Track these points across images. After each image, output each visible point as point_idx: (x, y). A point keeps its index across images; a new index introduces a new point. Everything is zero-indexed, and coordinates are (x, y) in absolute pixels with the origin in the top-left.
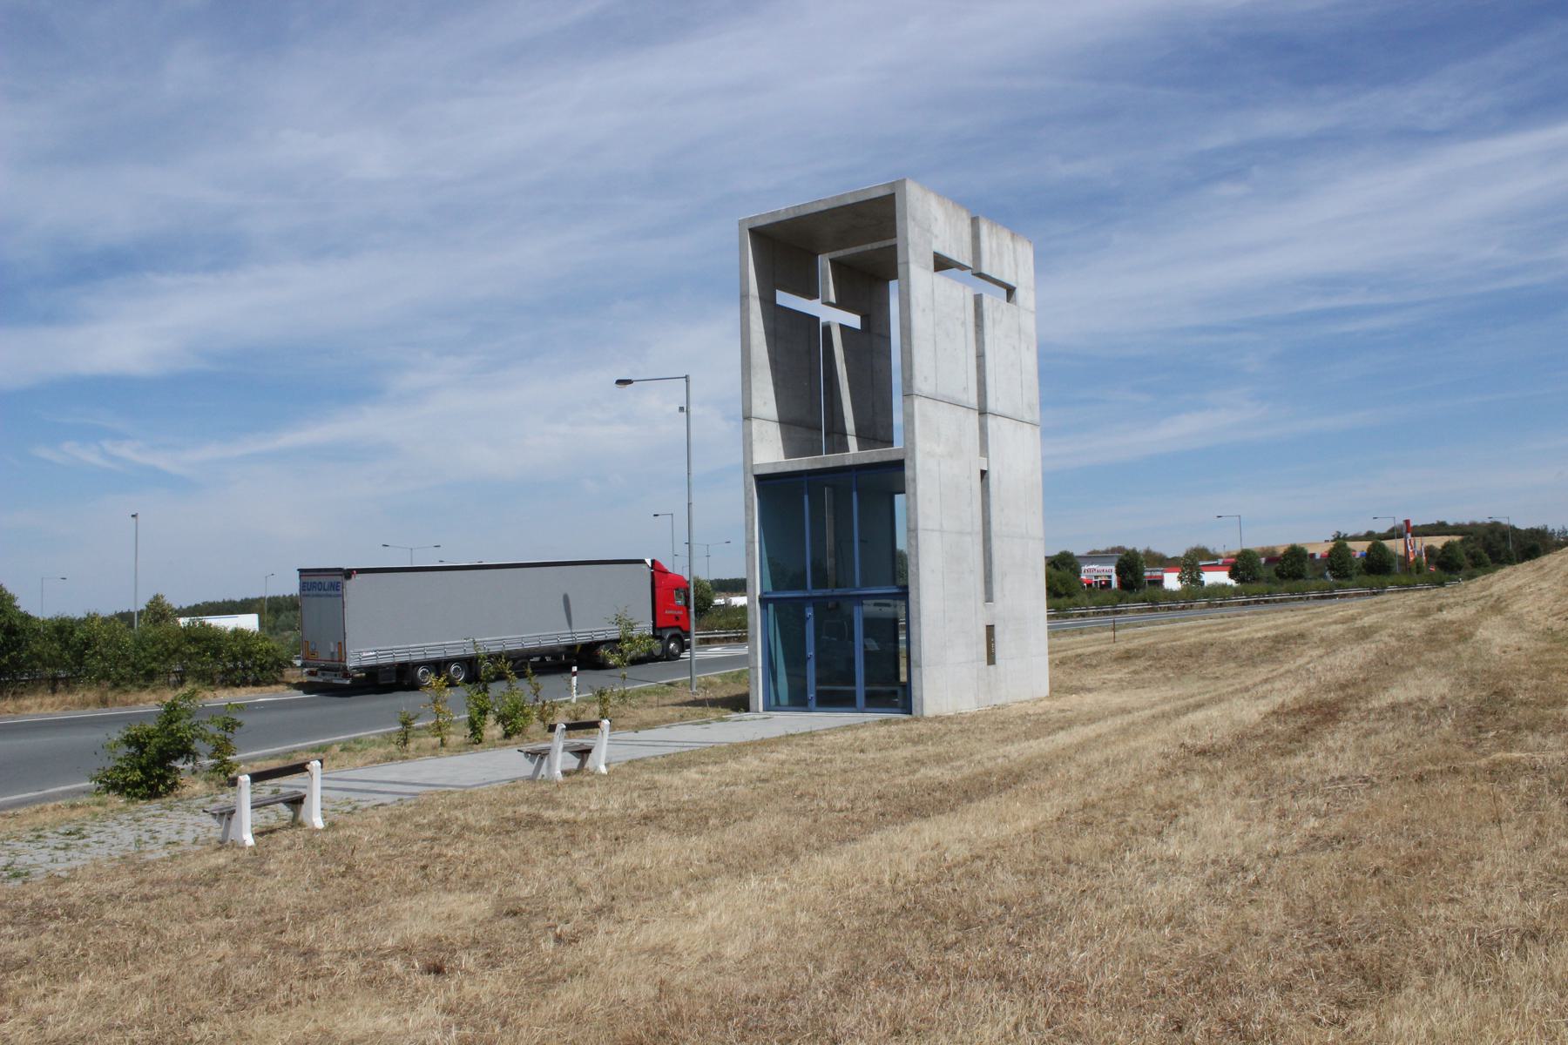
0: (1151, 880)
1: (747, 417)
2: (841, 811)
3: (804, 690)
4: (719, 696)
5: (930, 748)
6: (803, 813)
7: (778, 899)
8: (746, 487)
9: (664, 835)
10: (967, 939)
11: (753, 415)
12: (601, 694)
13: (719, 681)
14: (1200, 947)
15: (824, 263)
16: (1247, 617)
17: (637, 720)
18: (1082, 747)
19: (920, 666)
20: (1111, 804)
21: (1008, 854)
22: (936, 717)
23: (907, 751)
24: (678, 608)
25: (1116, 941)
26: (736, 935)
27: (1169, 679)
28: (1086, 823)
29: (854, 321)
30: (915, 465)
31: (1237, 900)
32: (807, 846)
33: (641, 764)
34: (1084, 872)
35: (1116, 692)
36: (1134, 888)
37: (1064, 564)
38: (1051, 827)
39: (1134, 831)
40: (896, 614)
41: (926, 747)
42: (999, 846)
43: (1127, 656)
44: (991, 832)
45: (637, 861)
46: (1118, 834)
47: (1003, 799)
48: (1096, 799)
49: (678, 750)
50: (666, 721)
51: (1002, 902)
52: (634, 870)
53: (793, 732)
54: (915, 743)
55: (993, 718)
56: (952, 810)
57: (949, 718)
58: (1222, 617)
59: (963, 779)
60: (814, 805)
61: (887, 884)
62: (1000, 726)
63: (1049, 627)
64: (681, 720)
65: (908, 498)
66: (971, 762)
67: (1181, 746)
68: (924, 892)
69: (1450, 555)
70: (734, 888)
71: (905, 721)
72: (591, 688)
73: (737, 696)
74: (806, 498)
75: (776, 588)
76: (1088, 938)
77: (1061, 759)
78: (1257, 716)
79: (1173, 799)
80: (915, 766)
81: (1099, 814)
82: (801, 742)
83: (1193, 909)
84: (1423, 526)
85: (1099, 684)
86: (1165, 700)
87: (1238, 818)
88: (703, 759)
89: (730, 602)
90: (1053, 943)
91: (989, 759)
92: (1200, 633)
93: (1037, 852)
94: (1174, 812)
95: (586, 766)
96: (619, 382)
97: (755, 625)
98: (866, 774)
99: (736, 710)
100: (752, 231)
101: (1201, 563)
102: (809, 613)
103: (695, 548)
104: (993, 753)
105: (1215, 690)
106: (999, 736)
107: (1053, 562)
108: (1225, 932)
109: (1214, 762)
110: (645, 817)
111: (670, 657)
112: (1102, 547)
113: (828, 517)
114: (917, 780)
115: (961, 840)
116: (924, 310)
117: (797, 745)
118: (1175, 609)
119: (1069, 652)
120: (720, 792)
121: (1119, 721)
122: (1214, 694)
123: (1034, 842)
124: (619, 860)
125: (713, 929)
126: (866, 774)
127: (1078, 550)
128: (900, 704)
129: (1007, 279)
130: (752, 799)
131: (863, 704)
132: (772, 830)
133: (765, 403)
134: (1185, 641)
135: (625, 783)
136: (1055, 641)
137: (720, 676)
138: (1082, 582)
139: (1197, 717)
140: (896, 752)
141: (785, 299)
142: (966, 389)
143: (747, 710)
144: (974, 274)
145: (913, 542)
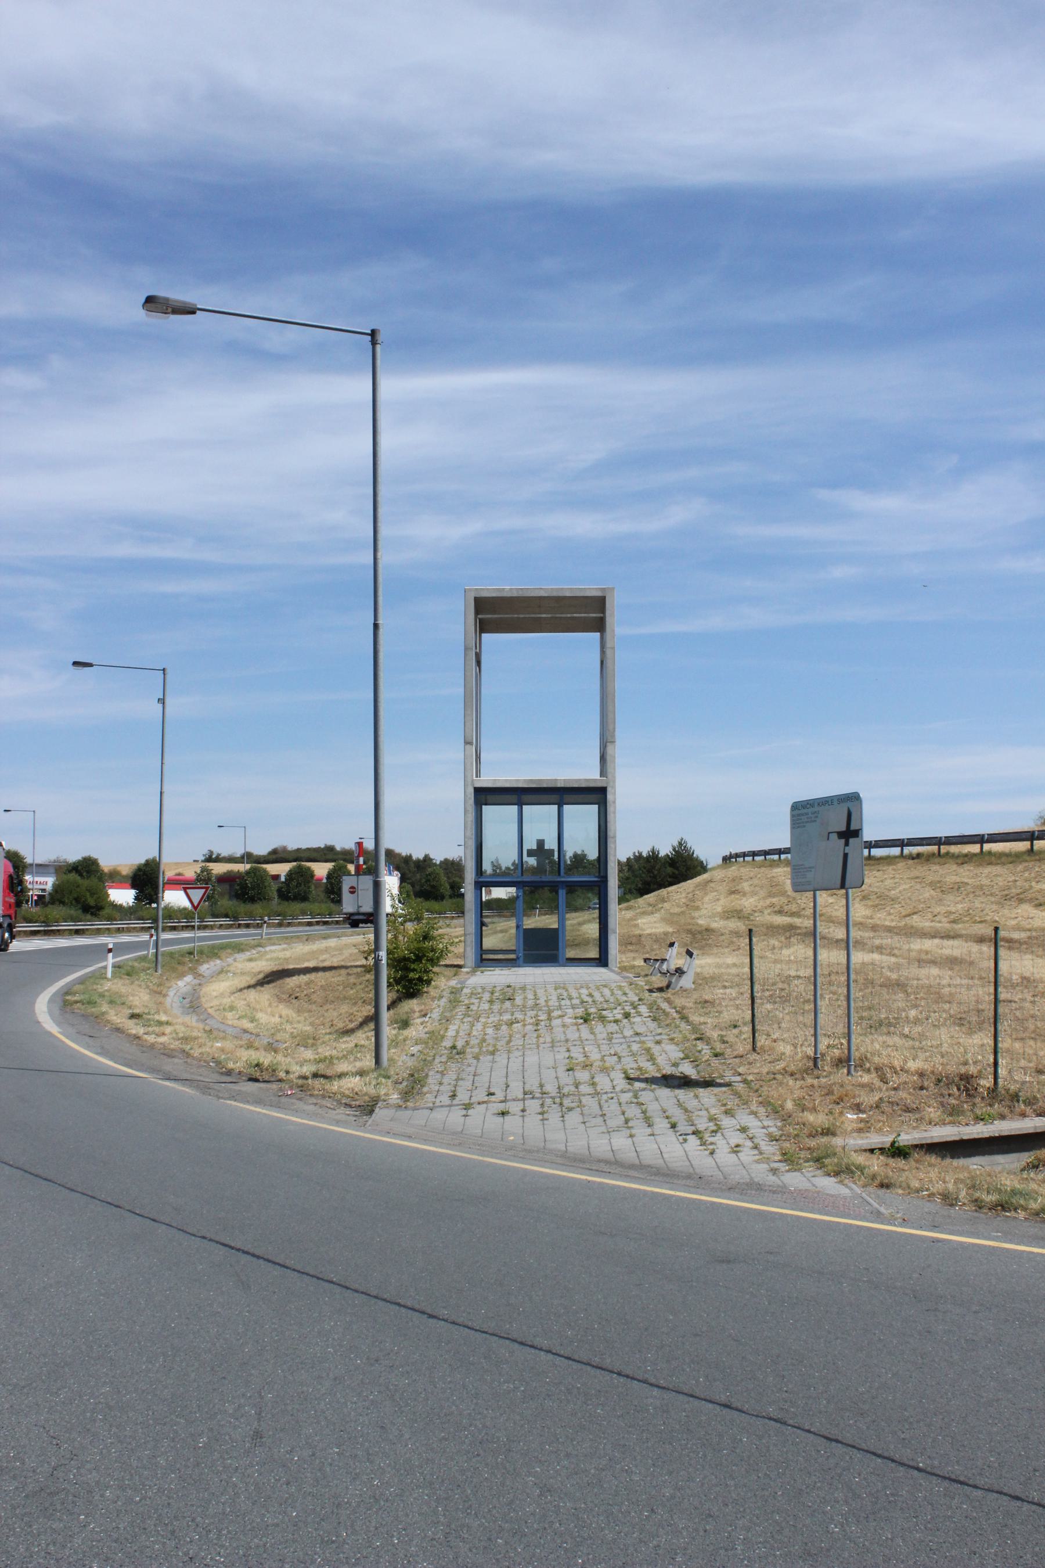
69: (434, 883)
84: (308, 849)
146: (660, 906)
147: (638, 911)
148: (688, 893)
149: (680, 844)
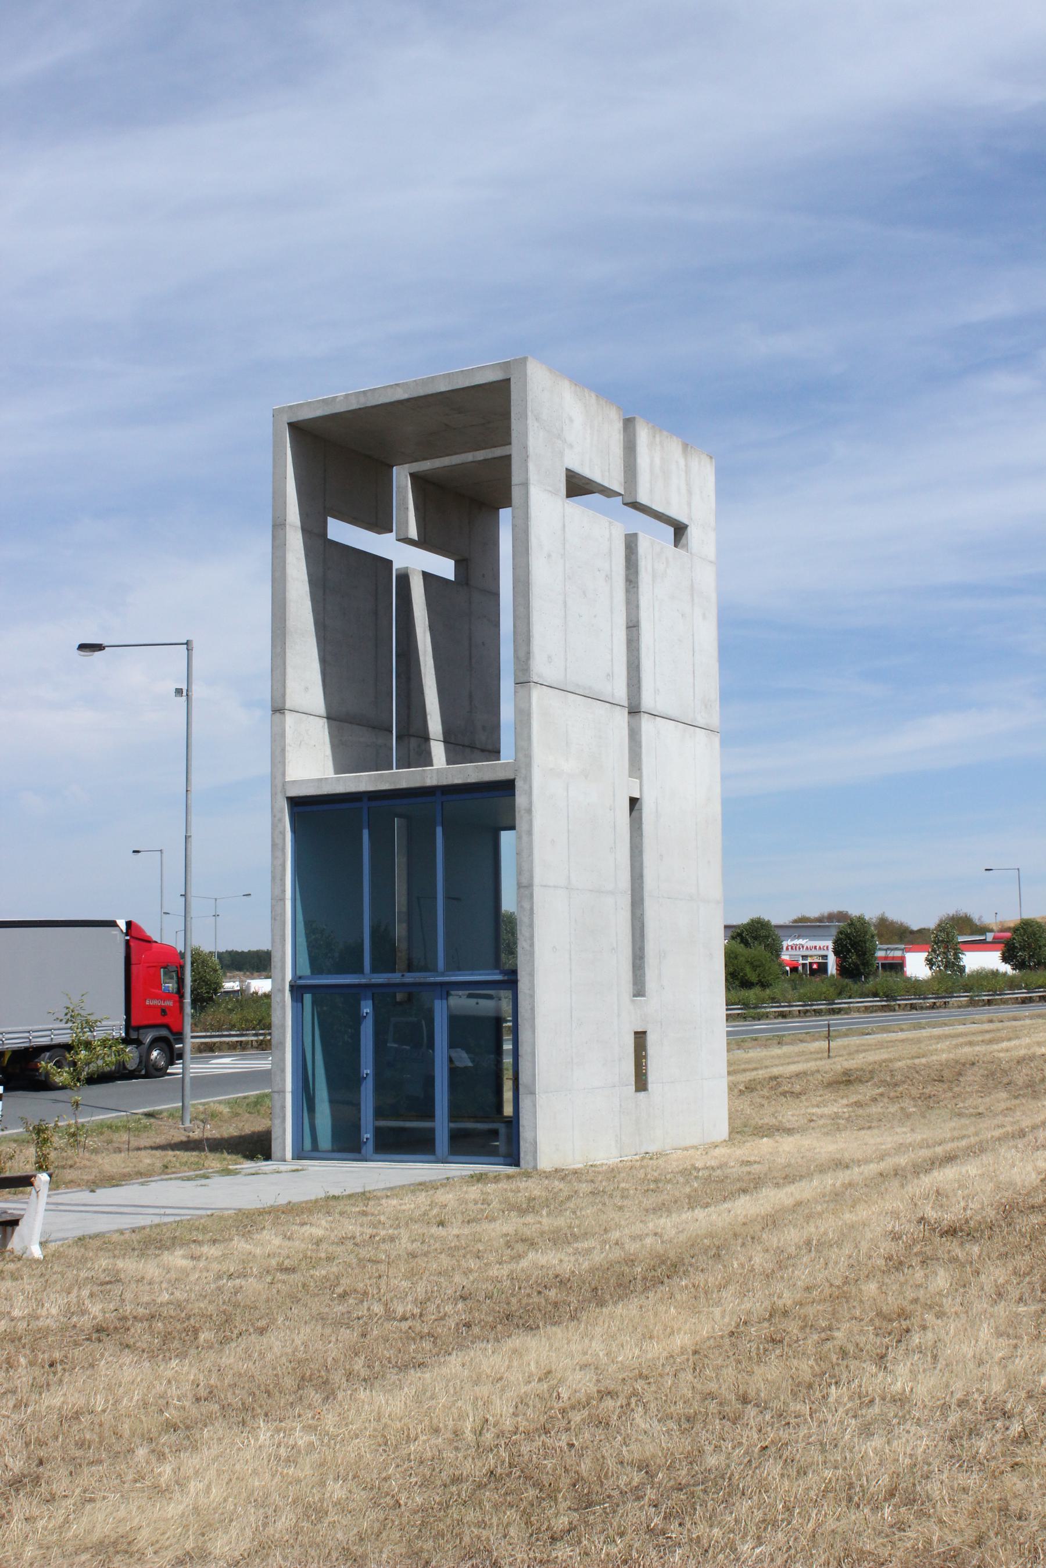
0: (866, 1431)
1: (279, 710)
2: (404, 1318)
3: (356, 1128)
4: (226, 1135)
5: (545, 1221)
6: (344, 1322)
7: (300, 1460)
8: (273, 816)
9: (127, 1358)
10: (586, 1523)
11: (288, 706)
12: (39, 1130)
13: (225, 1110)
14: (935, 1538)
15: (401, 478)
16: (1028, 1022)
17: (95, 1171)
18: (772, 1221)
19: (533, 1093)
20: (810, 1311)
21: (653, 1388)
22: (556, 1171)
23: (510, 1225)
24: (167, 996)
25: (811, 1525)
26: (231, 1521)
27: (908, 1116)
28: (773, 1340)
29: (444, 567)
30: (531, 787)
31: (993, 1464)
32: (349, 1375)
33: (98, 1243)
34: (768, 1417)
35: (827, 1134)
36: (841, 1444)
37: (755, 938)
38: (720, 1346)
39: (844, 1353)
40: (498, 1009)
41: (538, 1218)
42: (641, 1376)
43: (847, 1080)
44: (629, 1353)
45: (82, 1402)
46: (821, 1358)
47: (651, 1302)
48: (789, 1303)
49: (157, 1220)
50: (140, 1174)
51: (644, 1466)
52: (77, 1416)
53: (336, 1192)
54: (522, 1212)
55: (641, 1174)
56: (572, 1318)
57: (575, 1172)
58: (991, 1021)
59: (592, 1270)
60: (362, 1311)
61: (469, 1436)
62: (652, 1186)
63: (729, 1034)
64: (163, 1173)
65: (519, 838)
66: (605, 1242)
67: (919, 1222)
68: (525, 1450)
70: (233, 1443)
71: (509, 1177)
72: (24, 1121)
73: (254, 1133)
74: (366, 833)
75: (316, 968)
76: (769, 1523)
77: (740, 1241)
78: (1034, 1176)
79: (905, 1303)
80: (520, 1247)
81: (793, 1327)
82: (348, 1209)
83: (927, 1477)
85: (803, 1121)
86: (901, 1148)
87: (999, 1334)
88: (195, 1235)
89: (248, 986)
90: (716, 1530)
91: (633, 1238)
92: (956, 1046)
93: (699, 1386)
94: (905, 1324)
95: (9, 1247)
96: (83, 647)
97: (283, 1026)
98: (445, 1261)
99: (251, 1157)
100: (293, 426)
101: (961, 939)
102: (367, 1008)
103: (194, 902)
104: (638, 1228)
105: (976, 1134)
106: (649, 1202)
107: (740, 935)
108: (973, 1515)
109: (968, 1246)
110: (99, 1330)
111: (149, 1071)
112: (813, 913)
113: (400, 862)
114: (523, 1270)
115: (583, 1367)
116: (549, 556)
117: (341, 1214)
118: (922, 1008)
119: (760, 1072)
120: (219, 1288)
121: (831, 1181)
122: (973, 1140)
123: (695, 1369)
124: (53, 1399)
125: (196, 1509)
126: (445, 1261)
127: (778, 916)
128: (503, 1149)
129: (674, 513)
130: (268, 1300)
131: (446, 1149)
132: (296, 1349)
133: (307, 689)
134: (935, 1058)
135: (70, 1274)
136: (740, 1054)
137: (228, 1103)
138: (781, 965)
139: (945, 1176)
140: (492, 1225)
141: (340, 531)
142: (610, 676)
143: (268, 1157)
144: (625, 504)
145: (526, 905)
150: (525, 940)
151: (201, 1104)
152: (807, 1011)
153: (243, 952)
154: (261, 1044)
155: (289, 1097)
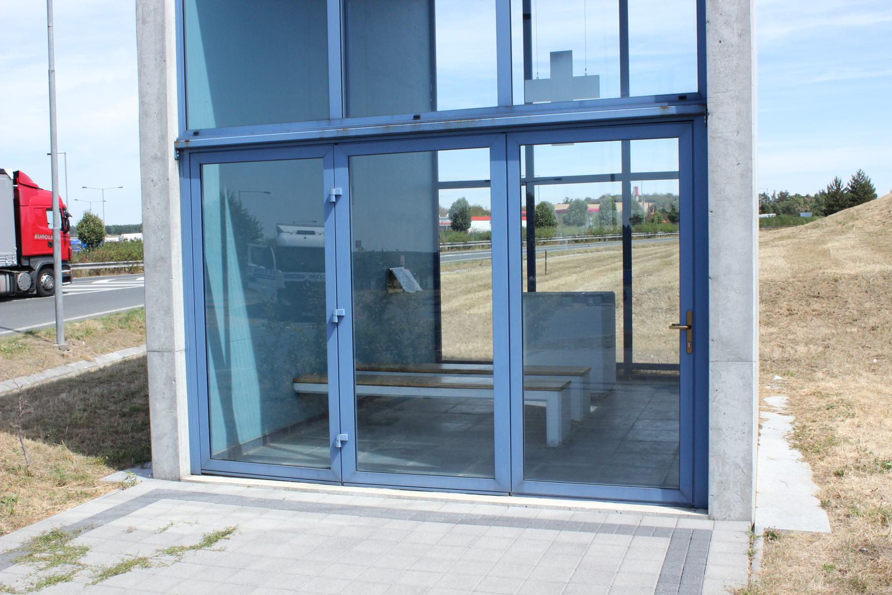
13: (99, 326)
111: (41, 292)
137: (102, 319)
146: (851, 224)
147: (826, 229)
148: (882, 210)
149: (859, 174)
150: (727, 23)
151: (77, 321)
152: (453, 248)
153: (121, 226)
154: (130, 270)
155: (181, 360)
